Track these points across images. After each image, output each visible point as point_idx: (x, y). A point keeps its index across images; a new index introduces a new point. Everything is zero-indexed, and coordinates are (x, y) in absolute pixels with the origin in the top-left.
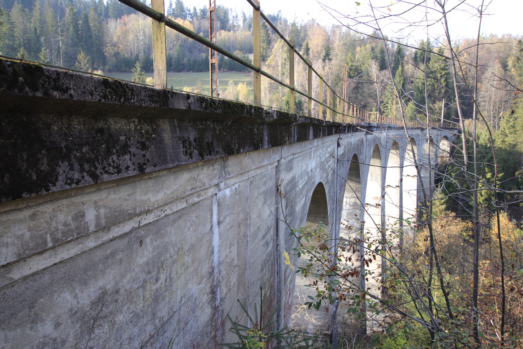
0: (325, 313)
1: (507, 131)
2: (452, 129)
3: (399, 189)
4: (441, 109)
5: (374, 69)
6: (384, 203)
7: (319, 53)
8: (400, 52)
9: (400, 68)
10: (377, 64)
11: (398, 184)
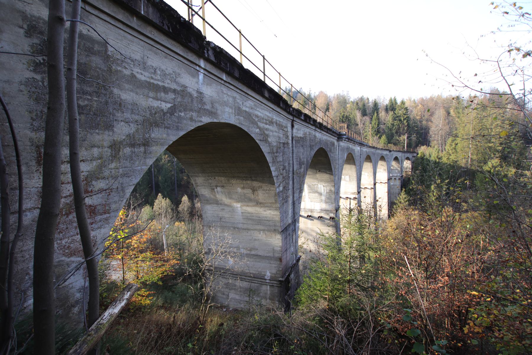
0: (279, 262)
1: (450, 152)
2: (412, 152)
3: (373, 190)
4: (404, 140)
5: (358, 115)
8: (376, 104)
9: (376, 114)
10: (360, 112)
11: (373, 187)
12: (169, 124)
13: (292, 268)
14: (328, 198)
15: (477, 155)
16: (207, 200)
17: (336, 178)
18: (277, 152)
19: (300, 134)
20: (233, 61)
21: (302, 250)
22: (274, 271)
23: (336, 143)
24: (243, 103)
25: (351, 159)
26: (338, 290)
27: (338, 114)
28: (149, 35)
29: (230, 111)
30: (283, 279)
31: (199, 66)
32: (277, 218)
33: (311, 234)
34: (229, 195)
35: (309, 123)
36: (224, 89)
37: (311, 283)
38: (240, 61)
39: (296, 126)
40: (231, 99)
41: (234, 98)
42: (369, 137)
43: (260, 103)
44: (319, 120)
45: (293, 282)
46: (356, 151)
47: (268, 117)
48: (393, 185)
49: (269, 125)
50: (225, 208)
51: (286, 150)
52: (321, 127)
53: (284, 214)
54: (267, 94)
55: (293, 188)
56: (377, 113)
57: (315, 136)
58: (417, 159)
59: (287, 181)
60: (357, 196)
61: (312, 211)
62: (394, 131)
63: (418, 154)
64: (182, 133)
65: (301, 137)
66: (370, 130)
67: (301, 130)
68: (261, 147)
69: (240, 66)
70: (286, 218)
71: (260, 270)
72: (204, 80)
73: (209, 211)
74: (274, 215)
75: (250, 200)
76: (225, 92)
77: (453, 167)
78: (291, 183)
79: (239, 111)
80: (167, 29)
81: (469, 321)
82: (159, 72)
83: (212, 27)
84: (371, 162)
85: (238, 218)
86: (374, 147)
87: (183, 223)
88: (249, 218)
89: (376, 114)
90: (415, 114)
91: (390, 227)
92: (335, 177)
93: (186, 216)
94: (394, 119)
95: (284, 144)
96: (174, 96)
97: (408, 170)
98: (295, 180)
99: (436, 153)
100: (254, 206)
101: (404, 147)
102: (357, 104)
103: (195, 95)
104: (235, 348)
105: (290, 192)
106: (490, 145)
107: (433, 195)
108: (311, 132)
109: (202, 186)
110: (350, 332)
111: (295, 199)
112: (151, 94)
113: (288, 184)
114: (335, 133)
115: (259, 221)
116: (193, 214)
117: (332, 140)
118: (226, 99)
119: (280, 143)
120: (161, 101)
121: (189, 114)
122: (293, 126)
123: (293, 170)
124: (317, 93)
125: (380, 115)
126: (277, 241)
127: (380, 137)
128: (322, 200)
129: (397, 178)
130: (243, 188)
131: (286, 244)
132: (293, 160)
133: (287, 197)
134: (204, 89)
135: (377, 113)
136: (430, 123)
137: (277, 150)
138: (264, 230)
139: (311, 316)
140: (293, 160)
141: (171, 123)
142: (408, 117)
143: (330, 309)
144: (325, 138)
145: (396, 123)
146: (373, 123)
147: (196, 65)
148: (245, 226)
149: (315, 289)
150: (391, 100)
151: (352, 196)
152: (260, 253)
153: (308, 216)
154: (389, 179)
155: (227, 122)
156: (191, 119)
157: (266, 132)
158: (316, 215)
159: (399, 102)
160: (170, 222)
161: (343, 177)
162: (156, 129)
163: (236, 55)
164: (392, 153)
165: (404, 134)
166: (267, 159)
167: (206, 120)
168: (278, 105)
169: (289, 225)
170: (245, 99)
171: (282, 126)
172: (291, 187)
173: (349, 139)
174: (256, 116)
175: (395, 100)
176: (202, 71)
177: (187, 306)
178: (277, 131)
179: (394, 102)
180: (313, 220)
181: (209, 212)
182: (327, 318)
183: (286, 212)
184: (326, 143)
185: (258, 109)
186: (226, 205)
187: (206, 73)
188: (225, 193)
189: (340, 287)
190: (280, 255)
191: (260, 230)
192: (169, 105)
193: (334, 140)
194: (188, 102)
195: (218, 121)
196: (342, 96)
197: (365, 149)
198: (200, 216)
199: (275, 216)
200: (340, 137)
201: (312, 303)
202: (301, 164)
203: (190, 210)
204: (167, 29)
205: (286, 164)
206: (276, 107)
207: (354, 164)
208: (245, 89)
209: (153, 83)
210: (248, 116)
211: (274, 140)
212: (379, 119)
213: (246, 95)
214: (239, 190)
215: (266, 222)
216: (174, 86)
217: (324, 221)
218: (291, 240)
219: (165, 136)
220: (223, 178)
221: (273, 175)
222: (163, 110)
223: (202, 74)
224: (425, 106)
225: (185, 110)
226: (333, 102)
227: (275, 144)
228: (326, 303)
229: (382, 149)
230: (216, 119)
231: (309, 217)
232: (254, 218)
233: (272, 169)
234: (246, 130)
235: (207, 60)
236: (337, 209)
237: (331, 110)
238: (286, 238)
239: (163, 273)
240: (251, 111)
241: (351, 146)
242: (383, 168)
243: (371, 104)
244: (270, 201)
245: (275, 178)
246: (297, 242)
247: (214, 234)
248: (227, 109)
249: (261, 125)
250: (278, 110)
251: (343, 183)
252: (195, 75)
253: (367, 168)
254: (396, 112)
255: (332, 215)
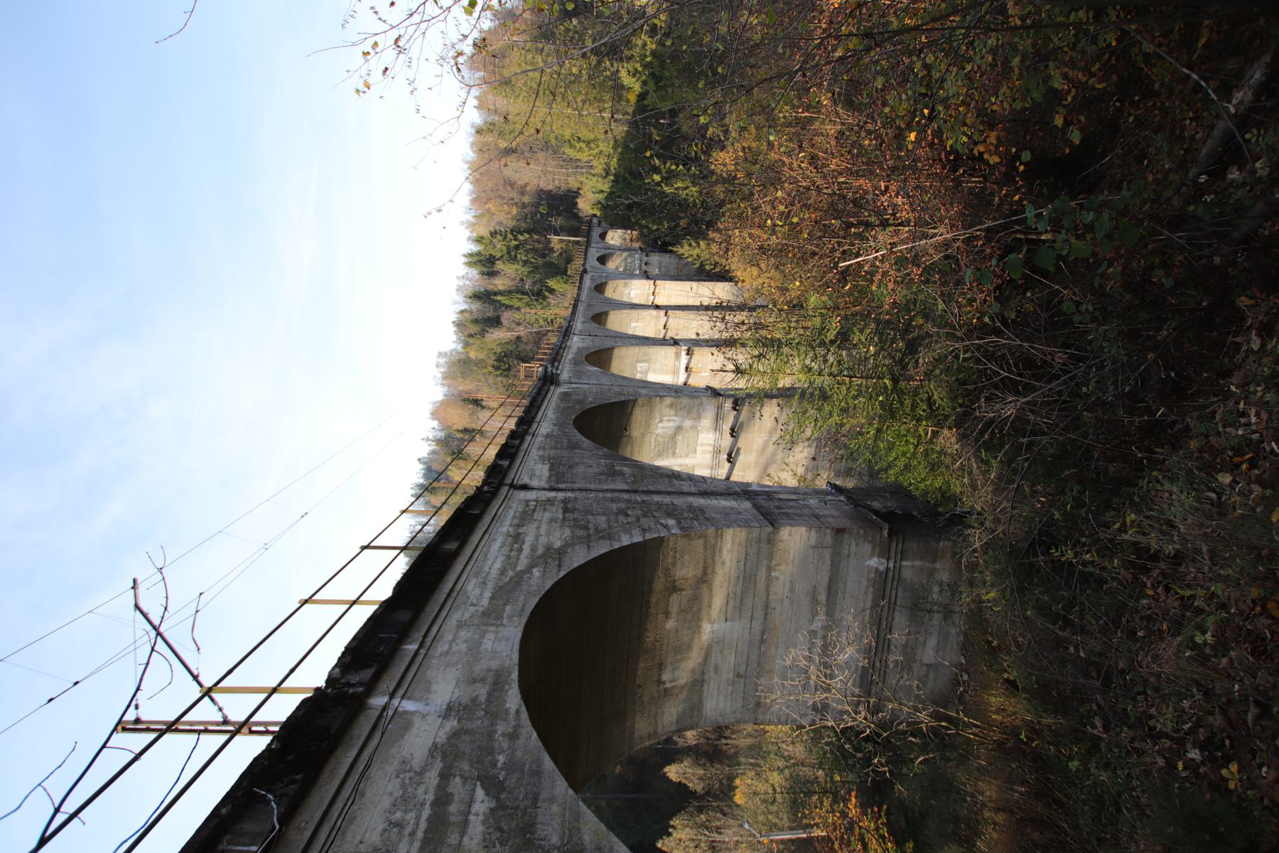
4: (562, 241)
5: (498, 336)
6: (686, 341)
7: (473, 414)
9: (499, 298)
11: (662, 313)
12: (526, 797)
13: (856, 505)
14: (689, 412)
15: (604, 101)
16: (692, 708)
17: (643, 391)
18: (587, 528)
19: (543, 470)
20: (373, 624)
21: (809, 477)
22: (867, 548)
23: (563, 389)
24: (473, 605)
25: (600, 358)
26: (914, 406)
27: (491, 379)
28: (308, 834)
29: (491, 636)
30: (886, 526)
31: (385, 708)
32: (742, 534)
33: (772, 454)
34: (682, 650)
35: (518, 448)
36: (439, 650)
37: (901, 463)
38: (376, 607)
39: (525, 480)
40: (464, 634)
41: (461, 625)
42: (549, 313)
43: (472, 563)
44: (511, 425)
45: (891, 504)
46: (581, 345)
47: (503, 544)
48: (660, 268)
49: (523, 543)
50: (713, 661)
51: (579, 506)
52: (526, 422)
53: (731, 519)
54: (452, 546)
55: (669, 493)
56: (495, 294)
57: (548, 436)
58: (605, 217)
59: (653, 507)
60: (685, 348)
61: (717, 451)
62: (540, 261)
63: (595, 216)
64: (548, 763)
65: (551, 470)
66: (533, 311)
67: (533, 468)
68: (575, 565)
69: (387, 607)
70: (740, 513)
71: (864, 583)
72: (418, 700)
73: (717, 704)
74: (733, 543)
75: (696, 598)
76: (446, 648)
77: (626, 147)
78: (656, 498)
79: (492, 615)
80: (294, 787)
81: (976, 152)
82: (399, 815)
83: (292, 671)
84: (606, 314)
85: (737, 630)
86: (575, 306)
87: (737, 782)
88: (738, 605)
89: (499, 298)
90: (506, 216)
91: (753, 278)
92: (640, 395)
93: (718, 770)
94: (514, 259)
95: (566, 510)
96: (457, 779)
97: (628, 237)
98: (651, 488)
99: (595, 179)
100: (711, 591)
101: (578, 243)
102: (471, 336)
103: (452, 724)
104: (1072, 649)
105: (679, 501)
106: (585, 77)
107: (685, 189)
108: (537, 444)
109: (656, 720)
110: (1011, 387)
111: (693, 489)
112: (453, 839)
113: (659, 505)
114: (540, 389)
115: (747, 578)
116: (713, 751)
117: (555, 398)
118: (463, 647)
119: (564, 519)
120: (469, 812)
121: (501, 742)
122: (525, 487)
123: (627, 491)
124: (435, 424)
125: (501, 288)
126: (794, 539)
127: (552, 291)
128: (694, 428)
129: (645, 259)
130: (667, 614)
131: (801, 516)
132: (603, 491)
133: (690, 508)
134: (439, 701)
135: (495, 294)
136: (528, 189)
137: (581, 527)
138: (769, 569)
139: (979, 467)
140: (603, 491)
141: (522, 789)
142: (512, 231)
143: (958, 424)
144: (551, 414)
145: (522, 256)
146: (517, 304)
147: (380, 716)
148: (759, 614)
149: (914, 455)
150: (469, 264)
151: (684, 359)
152: (824, 580)
153: (729, 461)
154: (646, 276)
155: (517, 647)
156: (513, 736)
157: (540, 552)
158: (727, 441)
159: (474, 248)
160: (734, 817)
161: (638, 376)
162: (541, 831)
163: (360, 616)
164: (588, 267)
165: (549, 241)
166: (603, 551)
167: (513, 699)
168: (478, 518)
169: (756, 507)
170: (461, 599)
171: (524, 512)
172: (667, 500)
173: (556, 357)
174: (502, 574)
175: (471, 255)
176: (395, 702)
177: (961, 775)
178: (536, 524)
179: (475, 259)
180: (739, 449)
181: (722, 706)
182: (982, 433)
183: (727, 513)
184: (562, 411)
185: (486, 569)
186: (705, 661)
187: (401, 692)
188: (678, 661)
189: (908, 402)
190: (828, 531)
191: (769, 579)
192: (480, 793)
193: (555, 394)
194: (472, 742)
195: (516, 668)
196: (449, 367)
197: (578, 325)
198: (721, 730)
199: (737, 540)
200: (549, 380)
201: (936, 459)
202: (612, 473)
203: (703, 761)
204: (294, 787)
205: (614, 506)
206: (480, 525)
207: (610, 351)
208: (440, 597)
209: (426, 832)
210: (504, 592)
211: (558, 534)
212: (510, 292)
213: (454, 595)
214: (670, 624)
215: (749, 564)
216: (432, 778)
217: (742, 424)
218: (791, 503)
219: (555, 808)
220: (641, 665)
221: (640, 539)
222: (492, 810)
223: (404, 703)
224: (491, 195)
225: (491, 752)
226: (461, 388)
227: (567, 532)
228: (946, 432)
229: (580, 289)
230: (510, 673)
231: (731, 459)
232: (739, 593)
233: (626, 541)
234: (537, 600)
235: (371, 687)
236: (715, 393)
237: (479, 396)
238: (788, 516)
239: (883, 837)
240: (490, 585)
241: (570, 356)
242: (620, 288)
243: (476, 306)
244: (701, 549)
245: (648, 537)
246: (794, 491)
247: (785, 695)
248: (488, 644)
249: (523, 563)
250: (487, 519)
251: (653, 378)
252: (405, 721)
253: (619, 322)
254: (498, 255)
255: (728, 404)
